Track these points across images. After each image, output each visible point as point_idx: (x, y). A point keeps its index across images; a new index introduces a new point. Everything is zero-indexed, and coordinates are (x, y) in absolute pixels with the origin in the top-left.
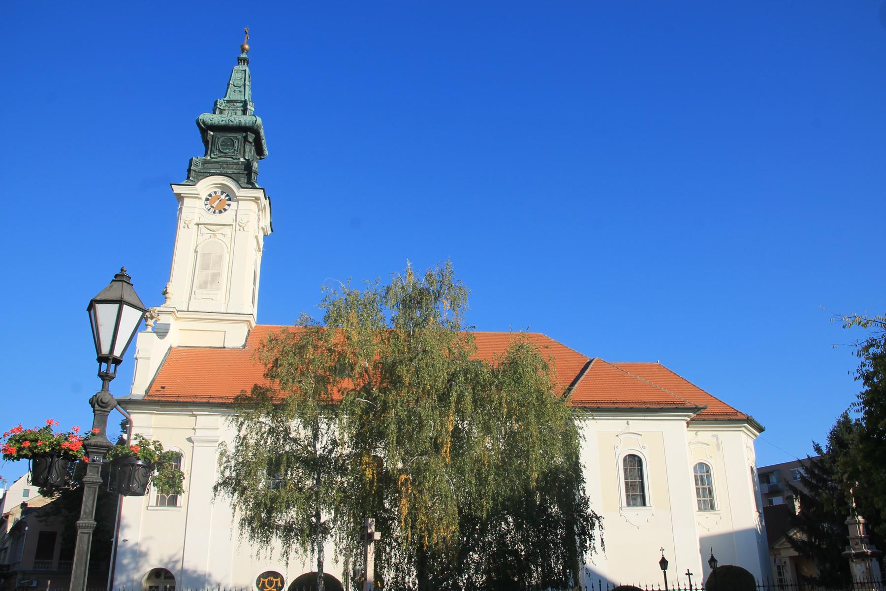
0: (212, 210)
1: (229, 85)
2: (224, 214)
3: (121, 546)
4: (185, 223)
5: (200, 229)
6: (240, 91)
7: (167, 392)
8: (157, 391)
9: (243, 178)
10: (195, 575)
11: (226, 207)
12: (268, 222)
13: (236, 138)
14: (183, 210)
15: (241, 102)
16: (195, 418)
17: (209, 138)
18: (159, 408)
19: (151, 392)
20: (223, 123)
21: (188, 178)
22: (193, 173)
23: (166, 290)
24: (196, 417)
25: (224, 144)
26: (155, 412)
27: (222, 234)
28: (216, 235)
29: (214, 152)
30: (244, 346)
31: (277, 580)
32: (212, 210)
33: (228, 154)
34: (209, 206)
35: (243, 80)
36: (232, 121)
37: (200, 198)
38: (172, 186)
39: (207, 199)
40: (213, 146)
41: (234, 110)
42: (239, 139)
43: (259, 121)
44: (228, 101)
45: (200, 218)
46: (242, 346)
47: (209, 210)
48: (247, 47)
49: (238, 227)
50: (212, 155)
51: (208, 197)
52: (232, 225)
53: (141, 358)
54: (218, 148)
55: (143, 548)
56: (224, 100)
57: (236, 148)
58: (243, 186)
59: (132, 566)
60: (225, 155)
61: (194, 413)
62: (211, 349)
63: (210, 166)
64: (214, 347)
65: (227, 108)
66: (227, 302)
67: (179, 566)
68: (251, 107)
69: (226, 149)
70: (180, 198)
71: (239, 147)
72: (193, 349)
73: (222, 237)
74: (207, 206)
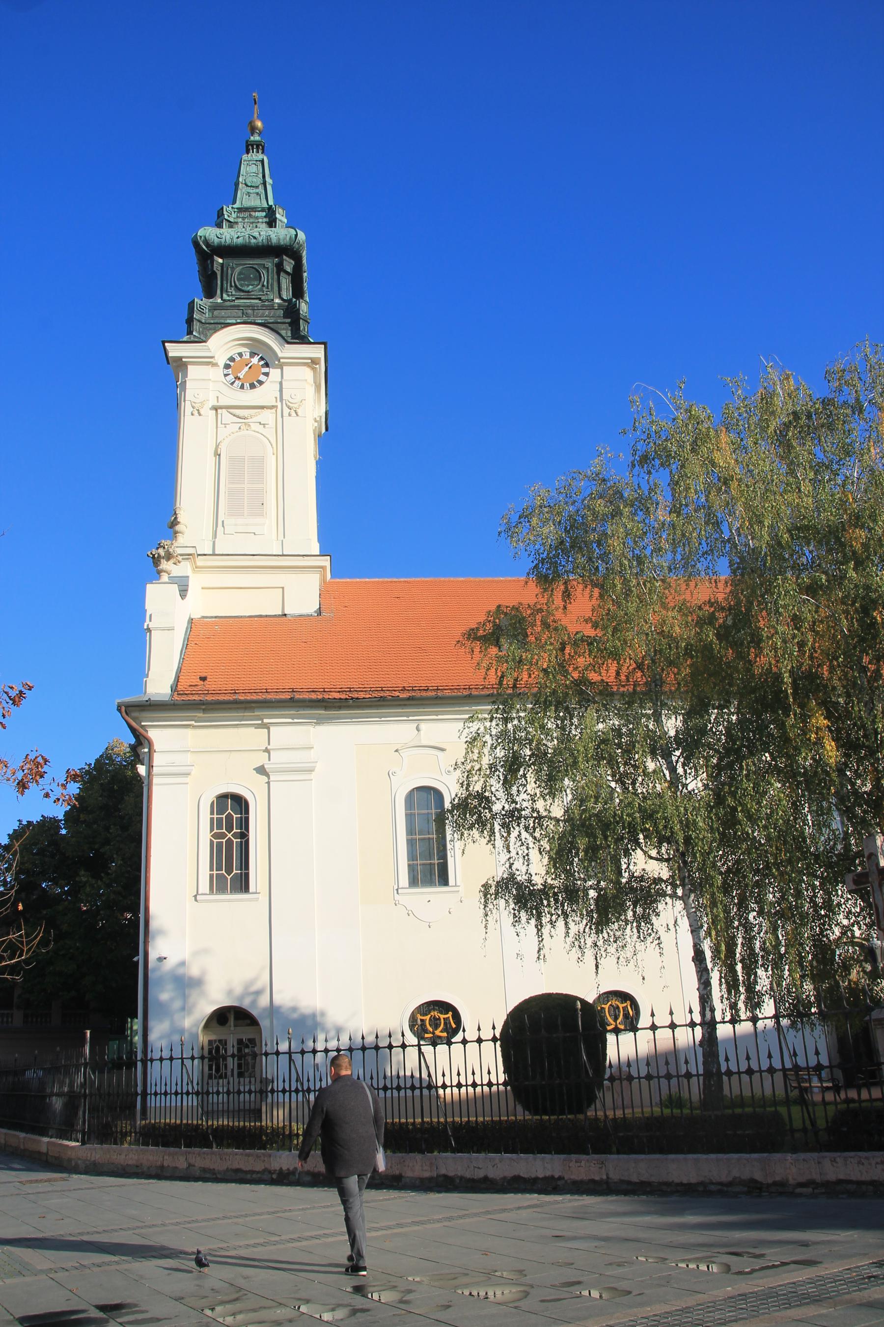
0: (238, 383)
1: (237, 184)
2: (259, 390)
3: (154, 970)
4: (193, 407)
5: (219, 416)
6: (257, 194)
7: (210, 685)
8: (190, 686)
9: (284, 329)
10: (295, 1016)
11: (262, 378)
12: (324, 410)
13: (264, 266)
14: (189, 385)
15: (263, 210)
16: (266, 730)
17: (217, 268)
18: (201, 715)
19: (180, 688)
20: (240, 241)
21: (190, 332)
22: (196, 325)
23: (176, 518)
24: (268, 729)
25: (244, 277)
26: (193, 723)
27: (260, 423)
28: (249, 425)
29: (227, 291)
30: (319, 612)
31: (625, 1005)
32: (238, 383)
33: (252, 293)
34: (231, 378)
35: (261, 176)
36: (255, 238)
37: (215, 365)
38: (166, 344)
39: (227, 366)
40: (225, 282)
41: (252, 223)
42: (268, 268)
43: (302, 236)
44: (240, 210)
45: (218, 397)
46: (315, 612)
47: (232, 384)
48: (259, 124)
49: (286, 411)
50: (225, 296)
51: (228, 362)
52: (277, 407)
53: (157, 629)
54: (233, 284)
55: (194, 971)
56: (232, 208)
57: (265, 283)
58: (289, 340)
59: (177, 1004)
60: (248, 295)
61: (266, 721)
62: (262, 619)
63: (223, 313)
64: (266, 616)
65: (240, 220)
66: (281, 537)
67: (264, 1001)
68: (280, 215)
69: (248, 286)
70: (180, 365)
71: (270, 280)
72: (231, 621)
73: (260, 428)
74: (228, 378)
